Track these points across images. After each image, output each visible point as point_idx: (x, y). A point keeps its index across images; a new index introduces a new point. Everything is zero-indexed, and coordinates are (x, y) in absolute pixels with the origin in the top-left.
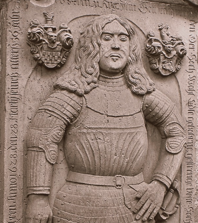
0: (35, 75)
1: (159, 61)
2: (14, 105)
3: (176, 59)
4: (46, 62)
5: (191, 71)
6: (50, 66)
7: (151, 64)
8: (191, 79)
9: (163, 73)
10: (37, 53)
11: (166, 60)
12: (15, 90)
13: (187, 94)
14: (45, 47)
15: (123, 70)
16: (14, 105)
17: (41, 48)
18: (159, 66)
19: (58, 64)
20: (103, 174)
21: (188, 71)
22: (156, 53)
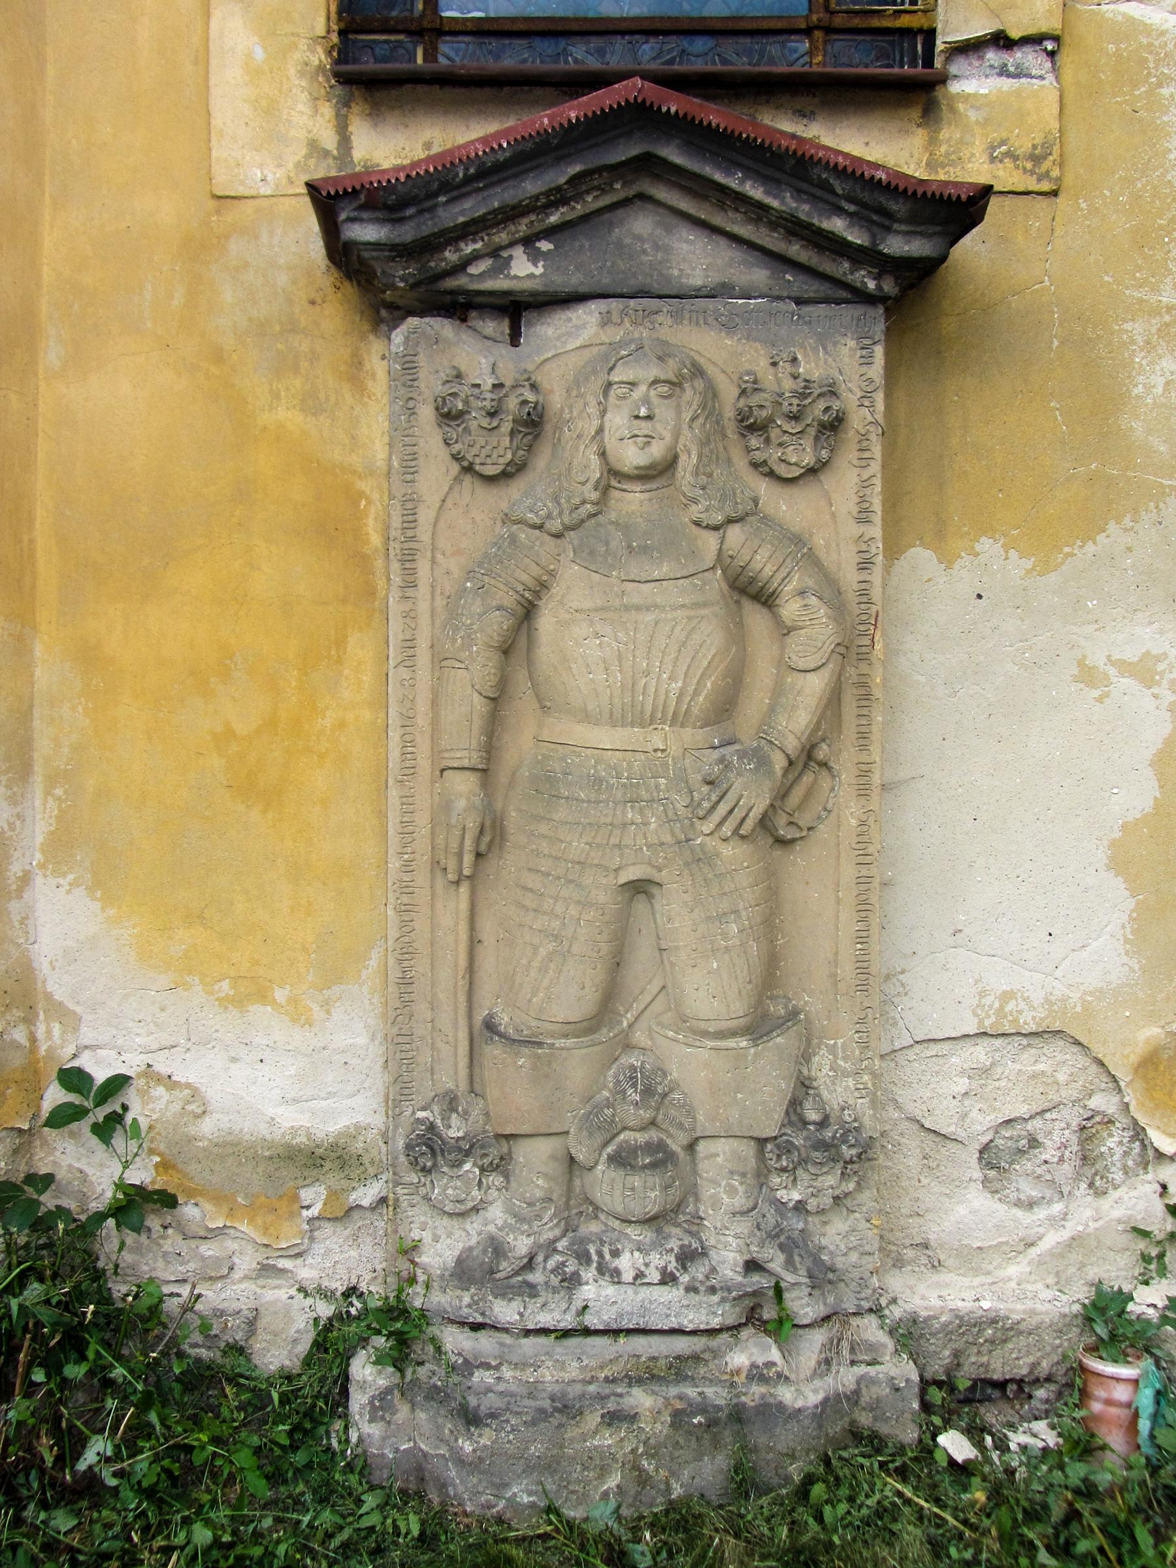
0: (466, 498)
1: (768, 441)
2: (408, 565)
3: (813, 433)
4: (478, 461)
5: (864, 463)
6: (490, 470)
7: (749, 452)
8: (865, 484)
9: (783, 471)
10: (456, 442)
11: (785, 438)
12: (410, 533)
13: (852, 522)
14: (473, 425)
15: (517, 886)
16: (408, 565)
17: (464, 429)
18: (773, 455)
19: (508, 464)
20: (622, 164)
21: (855, 462)
22: (755, 422)
